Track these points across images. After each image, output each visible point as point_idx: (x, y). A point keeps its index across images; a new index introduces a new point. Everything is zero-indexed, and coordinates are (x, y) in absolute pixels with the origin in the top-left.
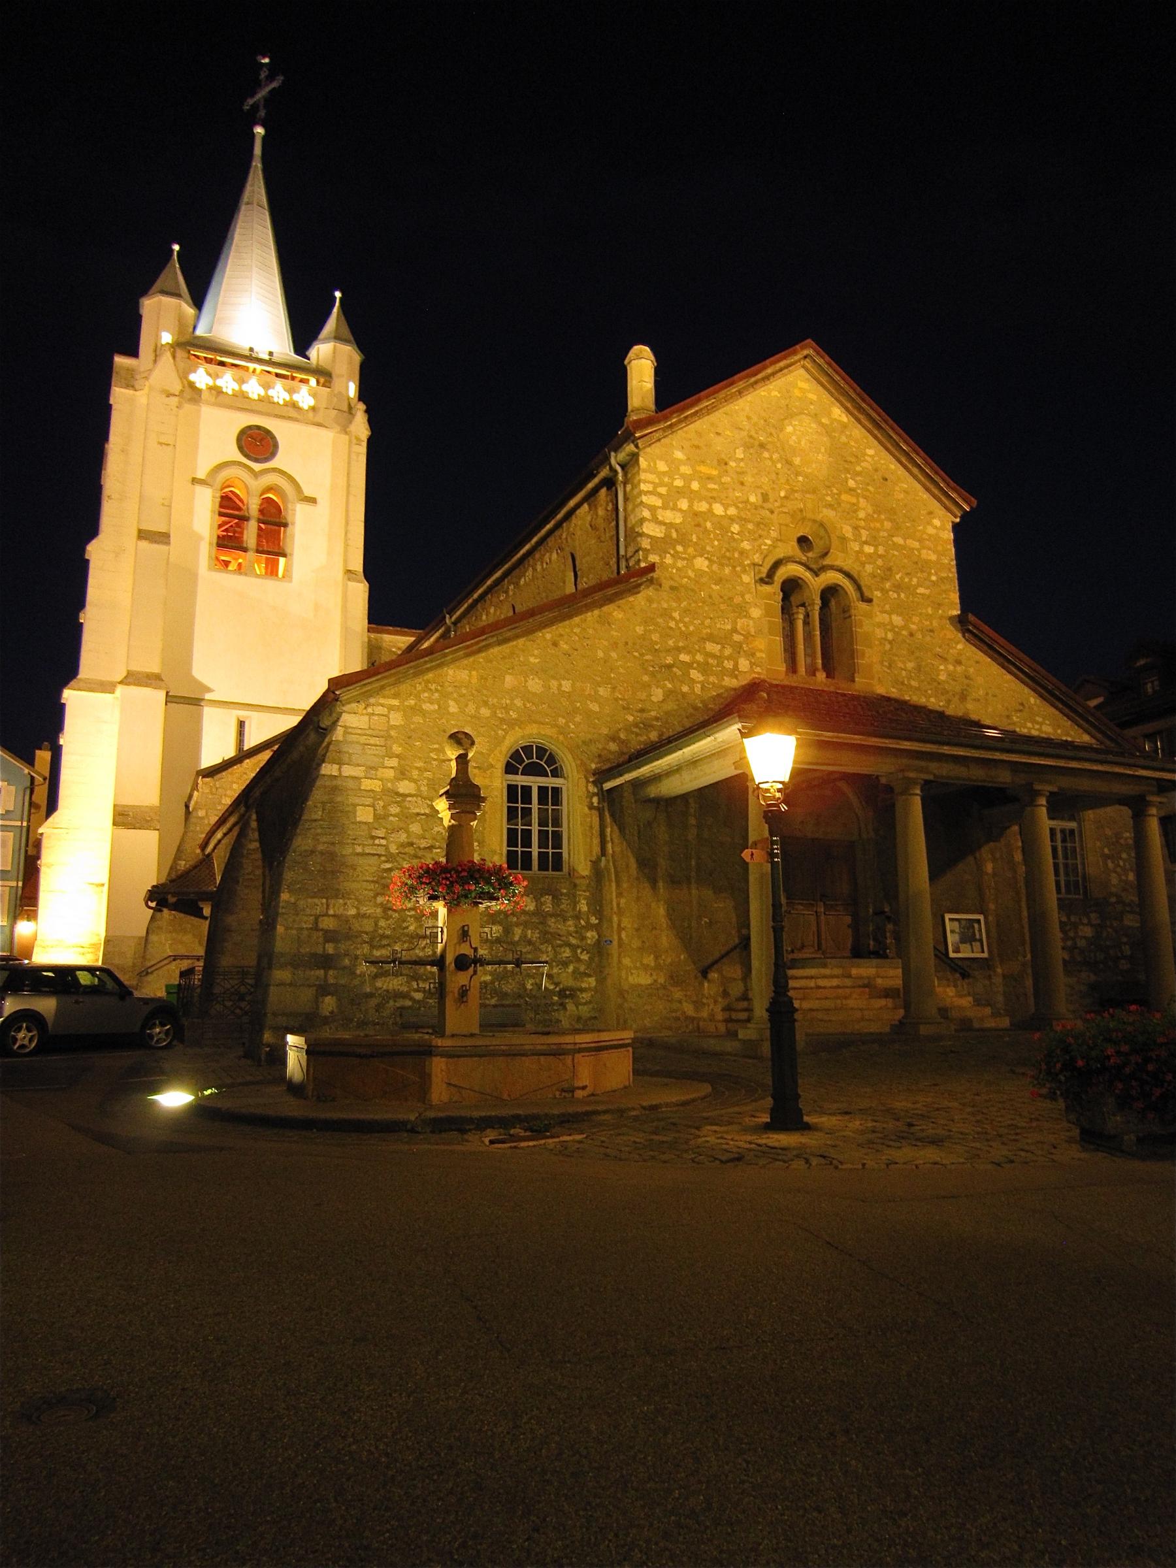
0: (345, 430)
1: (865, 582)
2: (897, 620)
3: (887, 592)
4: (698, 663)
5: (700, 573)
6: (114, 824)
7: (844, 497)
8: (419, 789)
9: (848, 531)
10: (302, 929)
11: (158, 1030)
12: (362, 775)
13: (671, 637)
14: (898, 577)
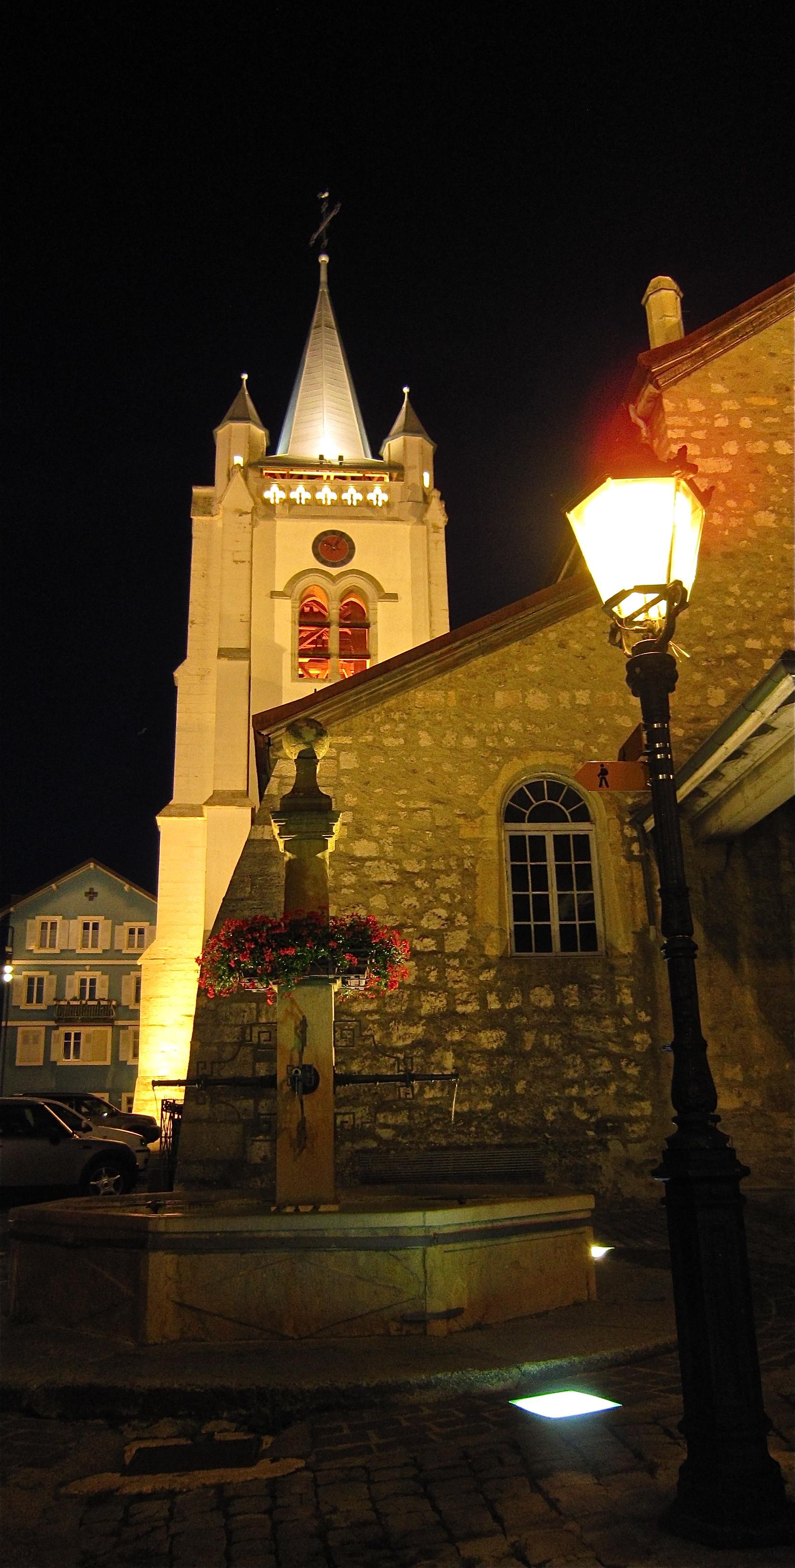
0: (421, 521)
5: (766, 532)
8: (381, 847)
13: (730, 620)
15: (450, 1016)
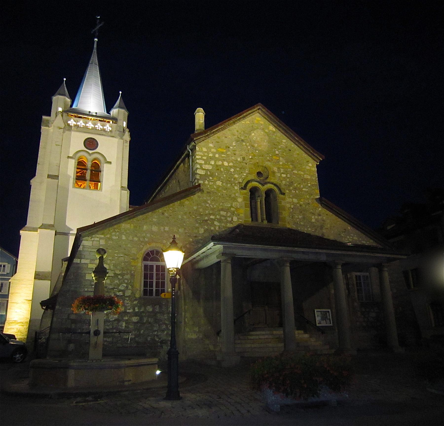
1: (283, 187)
2: (295, 200)
3: (291, 190)
4: (217, 219)
5: (219, 187)
6: (35, 278)
7: (274, 157)
9: (275, 169)
10: (63, 319)
11: (18, 356)
12: (89, 262)
14: (295, 185)
15: (125, 313)
